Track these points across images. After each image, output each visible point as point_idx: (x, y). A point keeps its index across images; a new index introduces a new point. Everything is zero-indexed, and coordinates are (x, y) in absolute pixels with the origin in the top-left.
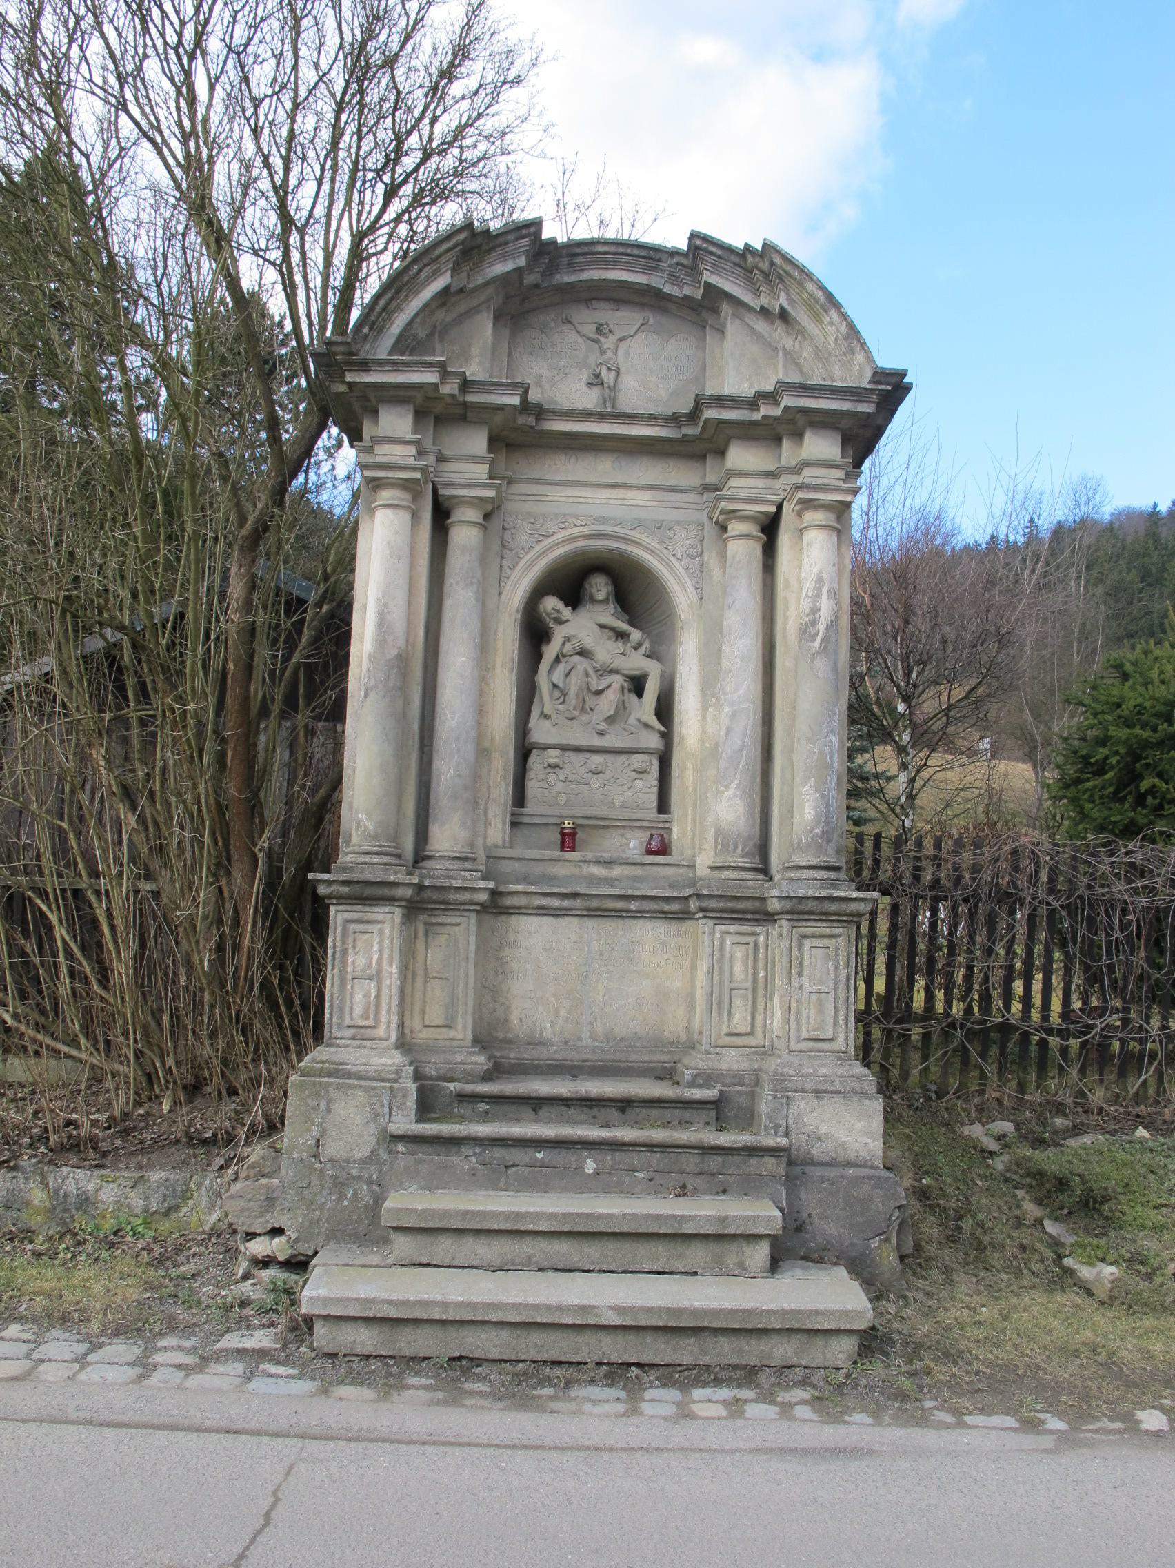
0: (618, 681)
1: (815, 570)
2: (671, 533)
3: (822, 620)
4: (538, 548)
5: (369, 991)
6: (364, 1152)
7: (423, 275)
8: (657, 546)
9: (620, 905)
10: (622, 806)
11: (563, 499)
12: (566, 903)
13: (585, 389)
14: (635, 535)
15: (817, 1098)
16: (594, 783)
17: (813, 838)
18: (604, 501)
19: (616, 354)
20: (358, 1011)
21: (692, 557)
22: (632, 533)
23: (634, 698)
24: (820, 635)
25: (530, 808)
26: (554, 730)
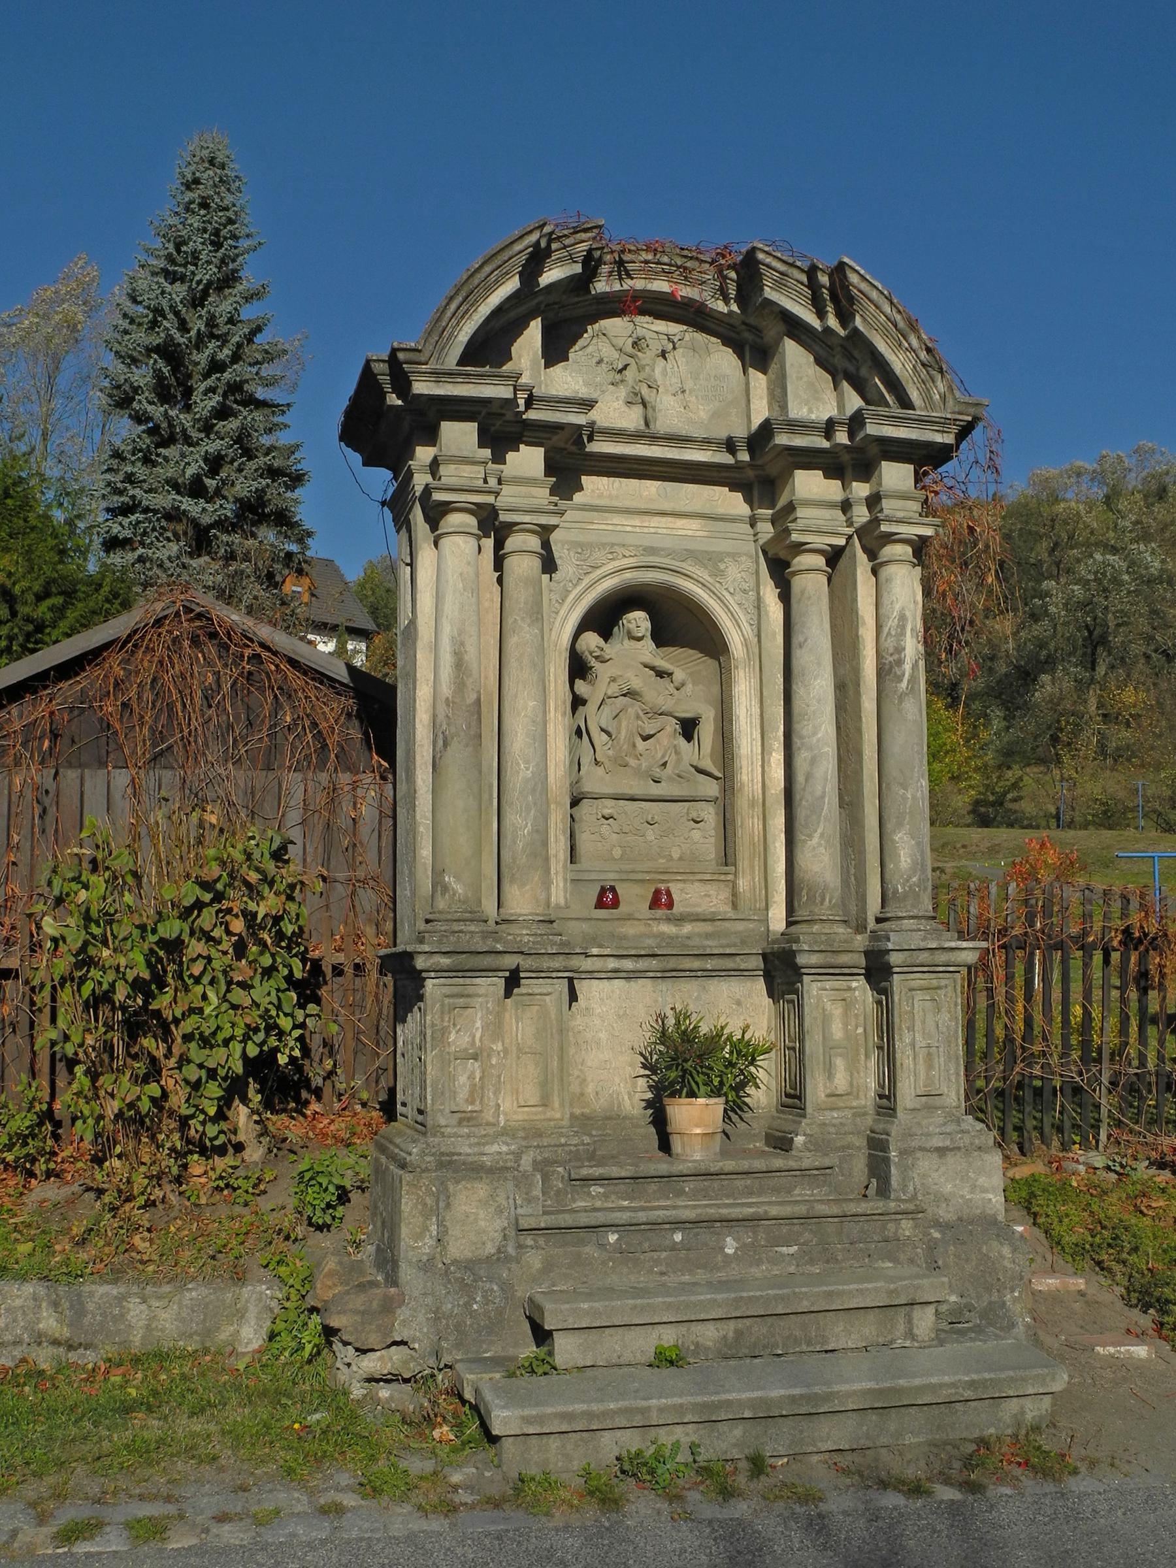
0: (672, 725)
1: (897, 607)
2: (722, 566)
3: (908, 660)
4: (586, 581)
5: (473, 1073)
6: (490, 1249)
7: (493, 277)
8: (709, 579)
9: (696, 964)
10: (681, 859)
11: (610, 528)
12: (642, 964)
13: (625, 408)
14: (687, 567)
15: (940, 1157)
16: (650, 834)
17: (910, 887)
18: (653, 530)
19: (653, 370)
20: (463, 1094)
21: (745, 591)
22: (683, 565)
23: (682, 741)
24: (907, 676)
25: (585, 863)
26: (607, 777)
